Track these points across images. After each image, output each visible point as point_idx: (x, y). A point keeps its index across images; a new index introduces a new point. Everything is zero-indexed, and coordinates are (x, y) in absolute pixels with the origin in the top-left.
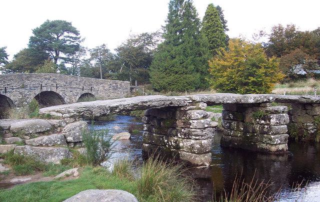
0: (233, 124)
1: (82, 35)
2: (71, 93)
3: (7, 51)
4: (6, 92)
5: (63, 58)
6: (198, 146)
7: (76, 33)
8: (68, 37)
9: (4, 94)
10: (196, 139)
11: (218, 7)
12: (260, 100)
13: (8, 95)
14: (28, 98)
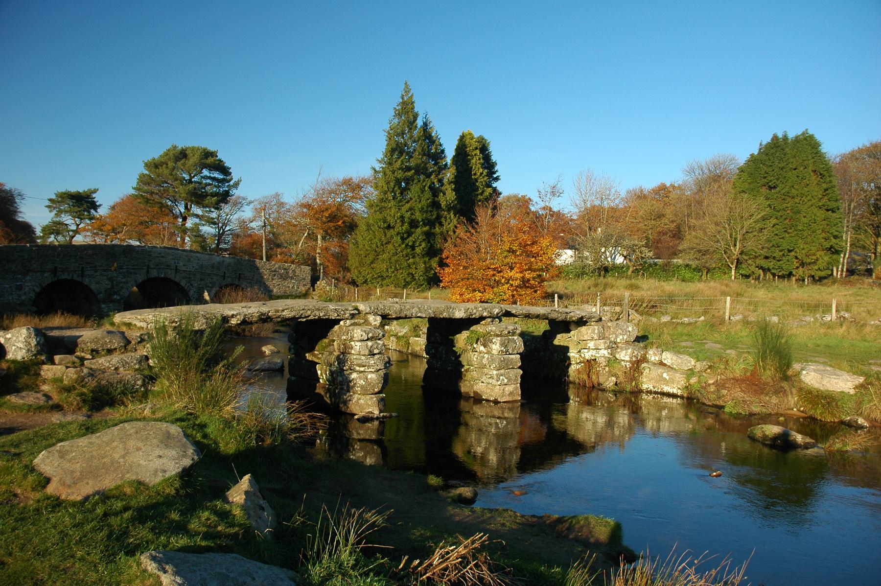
0: (440, 349)
1: (235, 176)
3: (98, 198)
4: (83, 276)
5: (197, 216)
6: (362, 382)
7: (225, 171)
8: (210, 178)
9: (80, 279)
10: (362, 372)
11: (147, 165)
13: (86, 281)
14: (122, 287)
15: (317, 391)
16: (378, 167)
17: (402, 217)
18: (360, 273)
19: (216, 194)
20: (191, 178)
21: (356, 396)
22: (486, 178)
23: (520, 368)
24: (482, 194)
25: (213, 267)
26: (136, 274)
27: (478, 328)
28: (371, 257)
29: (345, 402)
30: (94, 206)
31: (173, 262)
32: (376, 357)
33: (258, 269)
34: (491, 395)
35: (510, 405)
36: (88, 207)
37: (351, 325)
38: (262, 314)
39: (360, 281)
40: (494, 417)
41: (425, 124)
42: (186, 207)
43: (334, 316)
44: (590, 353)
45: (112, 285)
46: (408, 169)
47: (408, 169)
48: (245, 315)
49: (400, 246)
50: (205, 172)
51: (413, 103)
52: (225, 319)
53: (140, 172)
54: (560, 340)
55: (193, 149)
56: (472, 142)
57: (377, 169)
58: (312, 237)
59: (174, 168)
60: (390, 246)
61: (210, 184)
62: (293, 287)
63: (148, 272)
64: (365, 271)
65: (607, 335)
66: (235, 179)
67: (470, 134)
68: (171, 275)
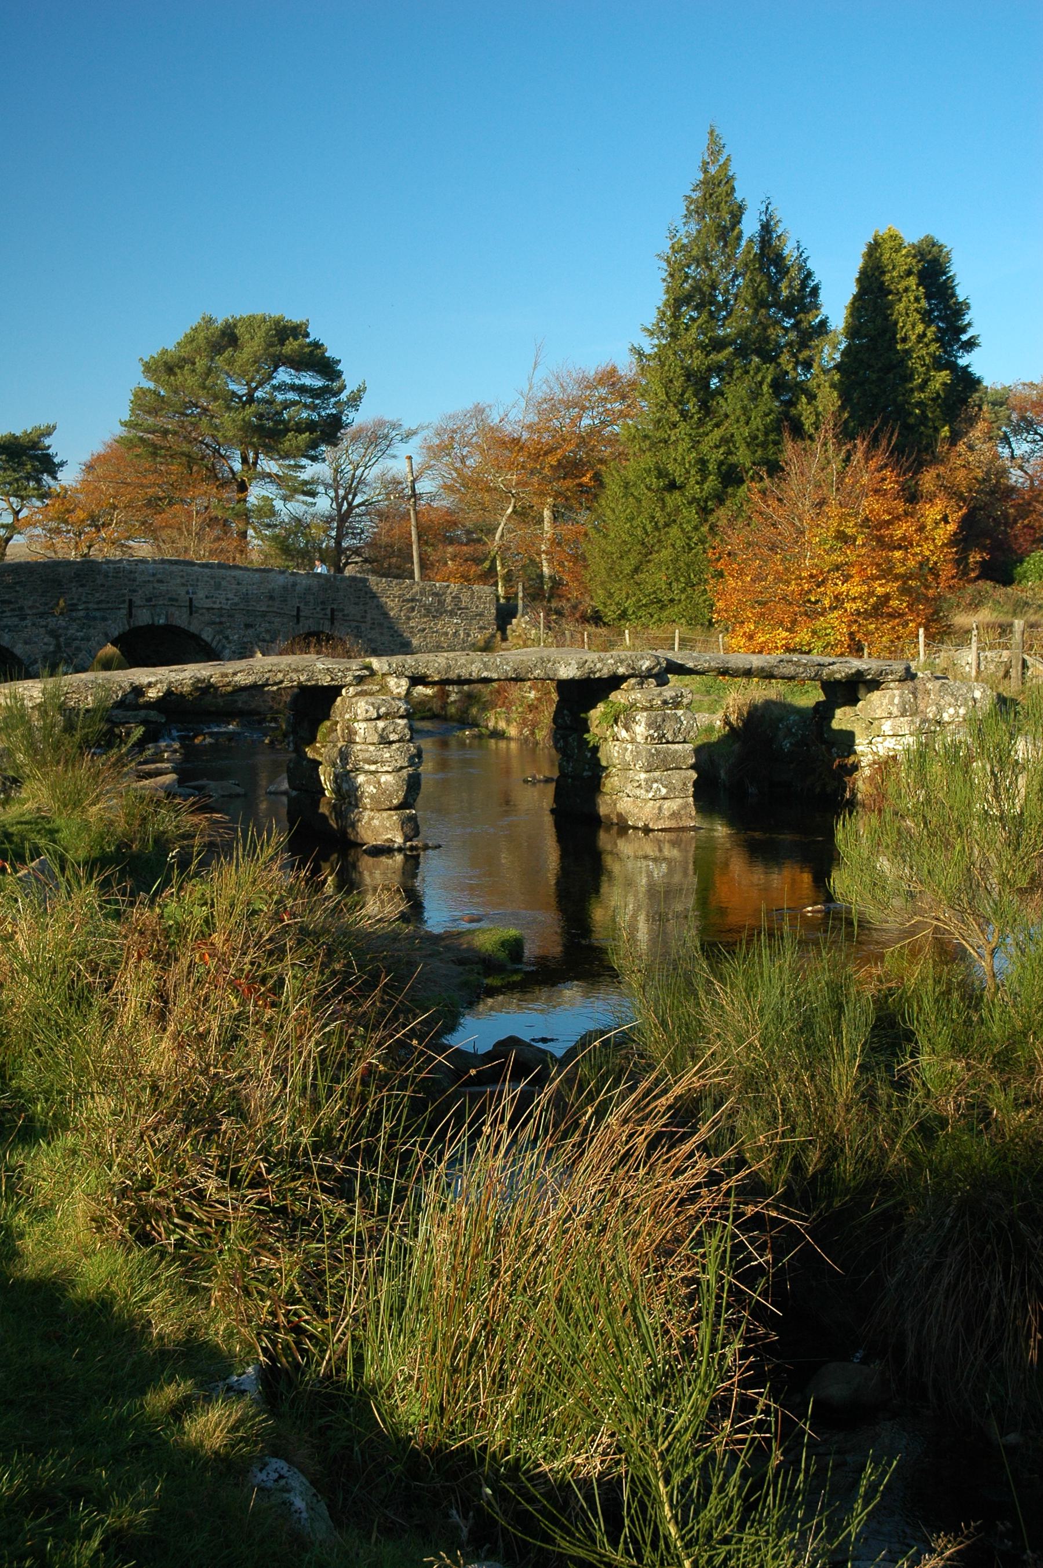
0: (570, 739)
1: (351, 380)
2: (250, 631)
3: (57, 446)
7: (328, 368)
8: (293, 388)
11: (149, 369)
12: (600, 670)
14: (78, 649)
15: (321, 810)
16: (648, 346)
17: (703, 462)
18: (611, 596)
19: (310, 426)
20: (252, 391)
21: (367, 814)
22: (933, 347)
23: (692, 767)
24: (922, 388)
25: (271, 598)
26: (104, 619)
27: (618, 697)
28: (633, 559)
29: (353, 825)
30: (49, 465)
31: (182, 591)
32: (395, 746)
33: (374, 596)
34: (639, 819)
35: (672, 836)
36: (35, 470)
37: (357, 694)
38: (199, 680)
39: (610, 613)
40: (646, 857)
41: (766, 228)
42: (245, 460)
43: (326, 681)
44: (886, 744)
45: (58, 646)
46: (718, 345)
47: (718, 345)
48: (171, 683)
49: (696, 528)
50: (284, 375)
51: (730, 180)
52: (138, 691)
53: (133, 386)
54: (842, 719)
55: (251, 322)
56: (899, 258)
57: (648, 350)
58: (525, 515)
59: (209, 371)
60: (674, 530)
61: (294, 403)
62: (456, 634)
63: (130, 614)
64: (620, 590)
65: (922, 707)
66: (351, 387)
67: (894, 237)
68: (180, 619)
